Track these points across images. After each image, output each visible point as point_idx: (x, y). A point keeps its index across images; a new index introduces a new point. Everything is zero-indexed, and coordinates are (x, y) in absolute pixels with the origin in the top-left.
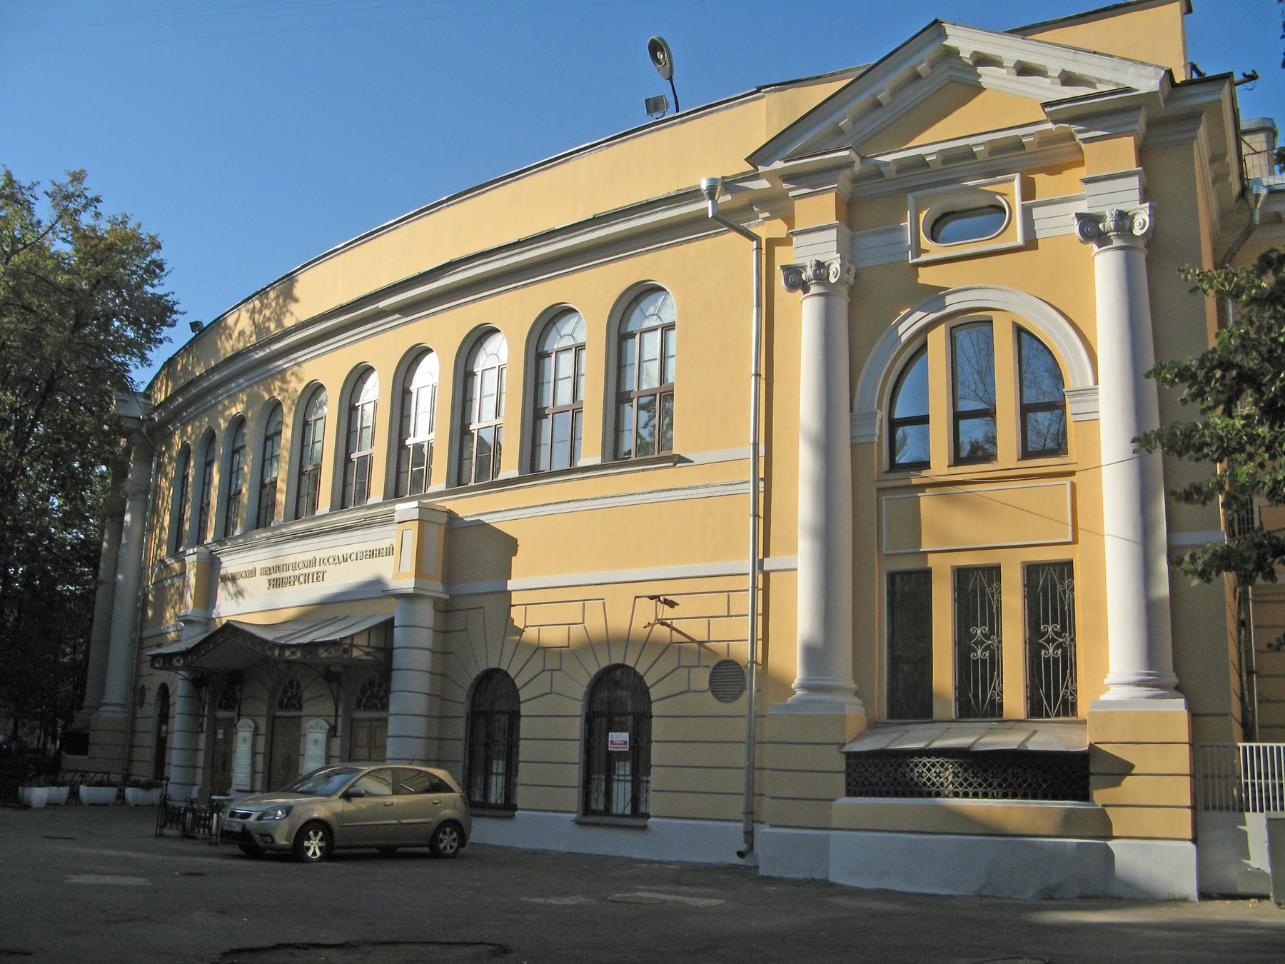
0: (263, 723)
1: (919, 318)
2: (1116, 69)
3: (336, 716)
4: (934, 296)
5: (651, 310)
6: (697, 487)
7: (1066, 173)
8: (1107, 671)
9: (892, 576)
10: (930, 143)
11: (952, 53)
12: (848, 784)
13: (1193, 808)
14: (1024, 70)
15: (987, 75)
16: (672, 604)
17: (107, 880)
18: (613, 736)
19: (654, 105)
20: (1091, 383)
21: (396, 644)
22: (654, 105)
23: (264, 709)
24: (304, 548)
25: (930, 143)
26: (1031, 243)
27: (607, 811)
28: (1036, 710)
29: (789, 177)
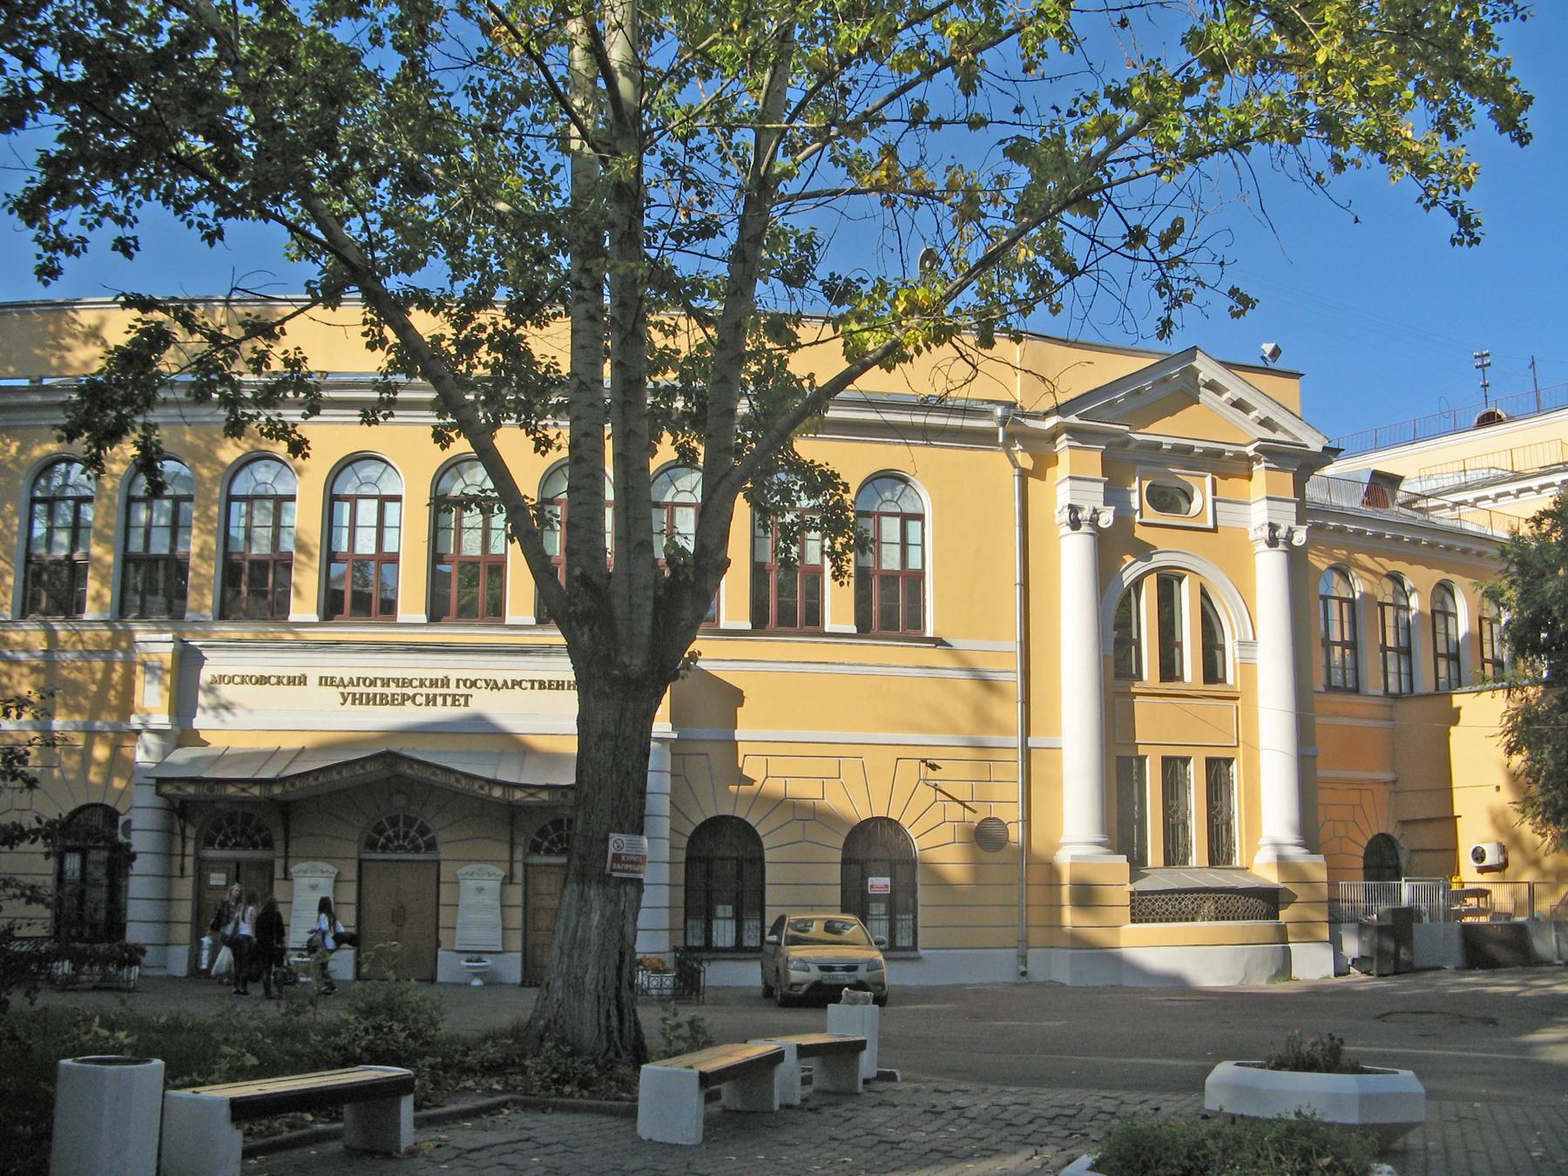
0: (352, 874)
1: (1140, 567)
3: (512, 861)
5: (888, 495)
8: (1260, 835)
10: (1166, 431)
11: (1194, 373)
14: (1239, 405)
15: (1205, 395)
16: (934, 767)
18: (872, 881)
21: (648, 789)
23: (352, 850)
25: (1166, 431)
28: (1168, 862)
29: (1072, 431)
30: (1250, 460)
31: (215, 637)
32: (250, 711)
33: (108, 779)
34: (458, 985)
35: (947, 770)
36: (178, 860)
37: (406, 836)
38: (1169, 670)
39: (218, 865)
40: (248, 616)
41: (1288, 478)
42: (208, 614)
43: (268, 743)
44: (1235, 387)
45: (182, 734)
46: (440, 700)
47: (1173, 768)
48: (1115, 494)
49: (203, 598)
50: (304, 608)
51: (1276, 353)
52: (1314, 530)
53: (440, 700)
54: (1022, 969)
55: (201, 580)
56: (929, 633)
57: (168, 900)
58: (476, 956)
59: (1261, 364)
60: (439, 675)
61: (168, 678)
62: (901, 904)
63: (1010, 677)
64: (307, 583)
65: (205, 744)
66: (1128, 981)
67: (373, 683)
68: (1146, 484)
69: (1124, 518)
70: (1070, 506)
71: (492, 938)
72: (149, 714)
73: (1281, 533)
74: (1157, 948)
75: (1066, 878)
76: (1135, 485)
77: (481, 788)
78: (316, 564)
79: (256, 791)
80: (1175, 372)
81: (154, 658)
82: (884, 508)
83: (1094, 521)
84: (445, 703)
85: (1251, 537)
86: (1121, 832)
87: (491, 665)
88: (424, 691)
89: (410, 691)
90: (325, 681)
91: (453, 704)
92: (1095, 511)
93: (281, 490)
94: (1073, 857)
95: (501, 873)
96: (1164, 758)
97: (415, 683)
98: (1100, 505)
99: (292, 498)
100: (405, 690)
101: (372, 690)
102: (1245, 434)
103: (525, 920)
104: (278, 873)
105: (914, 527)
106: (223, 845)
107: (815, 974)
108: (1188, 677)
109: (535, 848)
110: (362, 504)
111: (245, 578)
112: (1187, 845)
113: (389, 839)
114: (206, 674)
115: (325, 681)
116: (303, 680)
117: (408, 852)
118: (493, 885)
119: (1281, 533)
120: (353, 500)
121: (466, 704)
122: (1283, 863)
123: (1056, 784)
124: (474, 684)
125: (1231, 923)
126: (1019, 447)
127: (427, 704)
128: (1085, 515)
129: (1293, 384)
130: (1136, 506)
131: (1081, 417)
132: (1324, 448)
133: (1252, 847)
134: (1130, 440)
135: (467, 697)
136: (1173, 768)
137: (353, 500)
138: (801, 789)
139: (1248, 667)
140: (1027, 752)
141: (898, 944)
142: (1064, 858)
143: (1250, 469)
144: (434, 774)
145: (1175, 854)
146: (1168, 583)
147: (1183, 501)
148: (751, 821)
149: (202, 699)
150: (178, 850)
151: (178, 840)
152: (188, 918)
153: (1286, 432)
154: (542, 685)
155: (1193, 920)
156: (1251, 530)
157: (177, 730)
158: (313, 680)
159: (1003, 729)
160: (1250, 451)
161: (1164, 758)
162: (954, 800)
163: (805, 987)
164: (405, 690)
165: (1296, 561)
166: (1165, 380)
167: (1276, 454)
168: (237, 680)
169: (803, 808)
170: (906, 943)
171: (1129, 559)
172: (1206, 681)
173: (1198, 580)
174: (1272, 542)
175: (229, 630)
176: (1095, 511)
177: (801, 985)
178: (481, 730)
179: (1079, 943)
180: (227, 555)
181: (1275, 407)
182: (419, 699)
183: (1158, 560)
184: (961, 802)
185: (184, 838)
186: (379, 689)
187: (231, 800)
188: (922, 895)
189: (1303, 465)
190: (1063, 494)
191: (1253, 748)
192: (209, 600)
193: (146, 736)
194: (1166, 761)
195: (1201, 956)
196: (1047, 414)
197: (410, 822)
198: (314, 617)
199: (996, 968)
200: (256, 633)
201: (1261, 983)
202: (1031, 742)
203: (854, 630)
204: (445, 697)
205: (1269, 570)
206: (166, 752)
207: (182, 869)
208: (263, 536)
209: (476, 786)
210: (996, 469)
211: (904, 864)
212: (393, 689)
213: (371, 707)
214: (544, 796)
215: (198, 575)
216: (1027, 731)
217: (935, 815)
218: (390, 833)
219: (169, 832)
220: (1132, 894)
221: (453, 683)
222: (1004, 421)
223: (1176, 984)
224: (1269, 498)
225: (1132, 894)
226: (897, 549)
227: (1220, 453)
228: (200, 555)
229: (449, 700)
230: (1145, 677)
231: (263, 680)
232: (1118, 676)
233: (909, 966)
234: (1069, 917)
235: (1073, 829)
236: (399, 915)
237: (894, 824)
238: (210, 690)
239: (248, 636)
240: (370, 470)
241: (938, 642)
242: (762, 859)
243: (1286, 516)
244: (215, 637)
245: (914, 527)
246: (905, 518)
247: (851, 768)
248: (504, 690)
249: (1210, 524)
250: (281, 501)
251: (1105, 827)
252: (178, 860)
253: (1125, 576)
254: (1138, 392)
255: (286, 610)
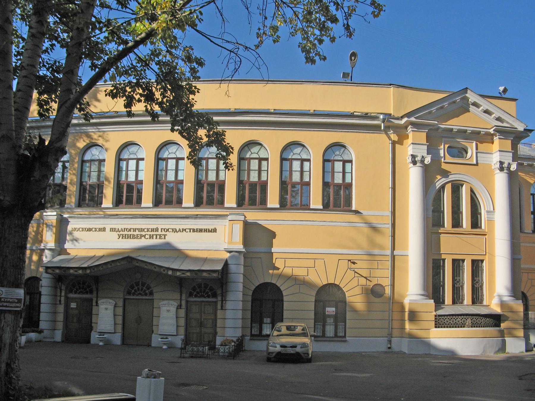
0: (121, 303)
2: (513, 121)
3: (181, 300)
4: (445, 174)
5: (337, 153)
6: (336, 222)
7: (484, 144)
9: (433, 259)
10: (455, 124)
11: (467, 99)
12: (436, 324)
13: (39, 320)
14: (487, 112)
15: (472, 108)
16: (354, 263)
17: (354, 375)
18: (328, 309)
19: (345, 75)
20: (492, 210)
22: (345, 75)
23: (121, 295)
24: (150, 223)
25: (455, 124)
26: (477, 164)
27: (324, 335)
29: (413, 124)
30: (492, 135)
31: (75, 213)
32: (84, 241)
33: (38, 268)
34: (158, 347)
35: (360, 264)
36: (59, 298)
37: (142, 290)
38: (457, 223)
39: (74, 300)
40: (88, 206)
41: (509, 142)
42: (73, 205)
43: (91, 254)
44: (485, 104)
45: (60, 249)
46: (155, 237)
47: (457, 264)
48: (432, 149)
49: (72, 199)
50: (108, 202)
51: (505, 91)
52: (519, 165)
53: (155, 237)
54: (389, 346)
55: (71, 193)
56: (353, 209)
57: (55, 313)
58: (165, 337)
59: (499, 96)
60: (154, 227)
61: (54, 229)
62: (340, 318)
63: (387, 226)
64: (109, 192)
65: (69, 254)
66: (433, 352)
67: (130, 230)
68: (447, 146)
69: (436, 159)
70: (412, 155)
71: (172, 330)
72: (47, 243)
73: (505, 165)
74: (444, 339)
75: (407, 309)
76: (442, 147)
77: (164, 271)
78: (112, 185)
79: (80, 272)
80: (458, 99)
81: (49, 221)
82: (336, 158)
83: (422, 161)
84: (156, 238)
85: (493, 168)
86: (434, 291)
87: (174, 223)
88: (149, 233)
89: (143, 233)
90: (112, 230)
91: (160, 238)
92: (423, 157)
93: (101, 158)
94: (410, 300)
95: (176, 304)
96: (453, 259)
97: (145, 230)
98: (425, 154)
99: (104, 160)
100: (141, 233)
101: (129, 233)
102: (489, 124)
103: (216, 322)
104: (94, 304)
105: (348, 165)
106: (76, 293)
107: (278, 349)
108: (464, 226)
109: (191, 295)
110: (130, 161)
111: (87, 192)
112: (463, 296)
113: (135, 291)
114: (70, 228)
115: (112, 230)
116: (104, 230)
117: (142, 295)
118: (173, 309)
119: (505, 165)
120: (127, 160)
121: (165, 238)
122: (502, 304)
123: (405, 271)
124: (168, 230)
125: (478, 328)
126: (392, 132)
127: (150, 238)
128: (418, 159)
129: (514, 103)
130: (442, 155)
131: (416, 118)
132: (525, 129)
133: (491, 297)
134: (439, 128)
135: (165, 235)
136: (457, 264)
137: (127, 160)
138: (300, 272)
139: (491, 222)
140: (393, 257)
141: (338, 335)
142: (407, 302)
143: (493, 139)
144: (146, 265)
145: (457, 299)
146: (456, 188)
147: (464, 153)
148: (278, 285)
149: (68, 238)
150: (59, 294)
151: (59, 290)
152: (62, 320)
153: (508, 123)
154: (194, 230)
155: (464, 327)
156: (493, 164)
157: (58, 249)
158: (108, 230)
159: (382, 248)
160: (492, 131)
161: (453, 259)
162: (362, 276)
163: (274, 354)
164: (141, 233)
165: (512, 176)
166: (454, 102)
167: (503, 132)
168: (81, 230)
169: (299, 280)
170: (341, 334)
171: (439, 177)
172: (453, 226)
173: (469, 186)
174: (501, 169)
175: (79, 211)
176: (423, 157)
177: (273, 353)
178: (169, 248)
179: (411, 336)
180: (81, 184)
181: (503, 112)
182: (147, 237)
183: (451, 178)
184: (365, 277)
185: (61, 290)
186: (132, 233)
187: (205, 279)
188: (349, 315)
189: (516, 137)
190: (410, 150)
191: (492, 256)
192: (73, 200)
193: (46, 251)
194: (454, 261)
195: (461, 343)
196: (402, 117)
197: (143, 284)
198: (111, 206)
199: (378, 345)
200: (90, 212)
201: (492, 355)
202: (395, 253)
203: (321, 207)
204: (157, 235)
205: (500, 181)
206: (53, 257)
207: (60, 301)
208: (94, 175)
209: (162, 270)
210: (381, 142)
211: (342, 303)
212: (137, 232)
213: (129, 240)
214: (188, 274)
215: (70, 190)
216: (393, 248)
217: (354, 283)
218: (136, 288)
219: (56, 288)
220: (436, 316)
221: (160, 230)
222: (383, 121)
223: (451, 354)
224: (500, 151)
225: (436, 316)
226: (341, 174)
227: (479, 133)
228: (71, 183)
229: (158, 237)
230: (446, 226)
231: (90, 230)
232: (434, 225)
233: (343, 344)
234: (408, 326)
235: (412, 287)
236: (139, 320)
237: (337, 286)
238: (71, 233)
239: (87, 213)
240: (133, 149)
241: (357, 212)
242: (282, 301)
243: (508, 158)
244: (75, 213)
245: (348, 165)
246: (345, 162)
247: (320, 264)
248: (179, 233)
249: (475, 162)
250: (101, 162)
251: (425, 287)
252: (59, 298)
253: (437, 184)
254: (442, 108)
255: (101, 203)
